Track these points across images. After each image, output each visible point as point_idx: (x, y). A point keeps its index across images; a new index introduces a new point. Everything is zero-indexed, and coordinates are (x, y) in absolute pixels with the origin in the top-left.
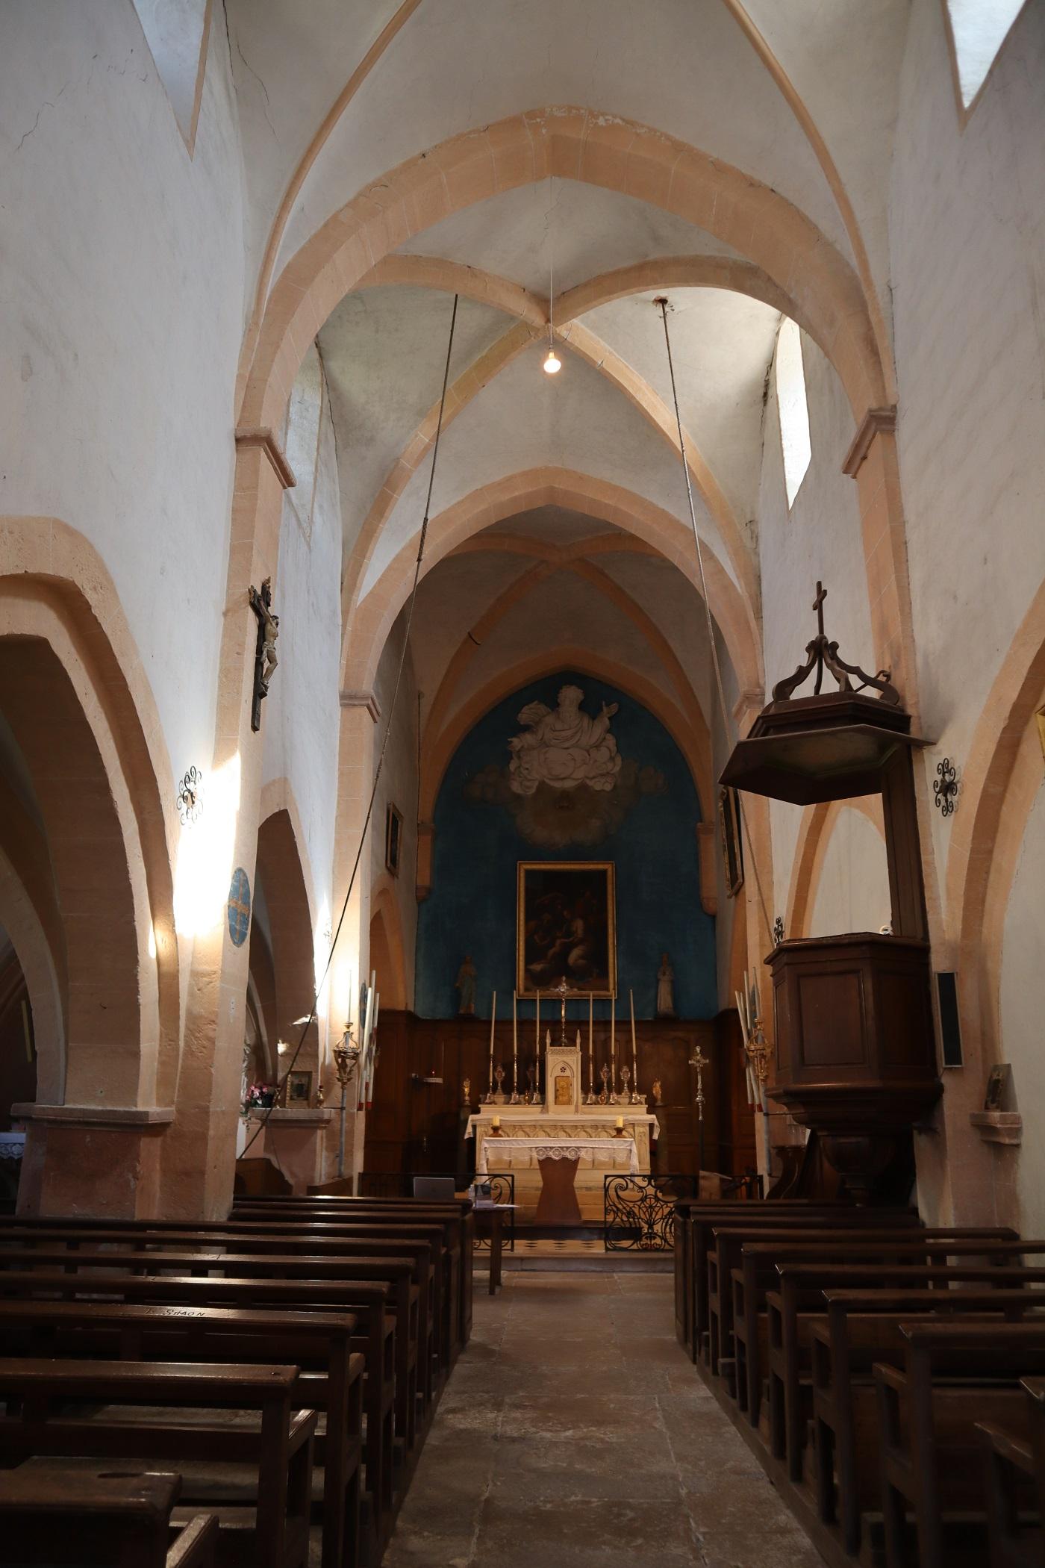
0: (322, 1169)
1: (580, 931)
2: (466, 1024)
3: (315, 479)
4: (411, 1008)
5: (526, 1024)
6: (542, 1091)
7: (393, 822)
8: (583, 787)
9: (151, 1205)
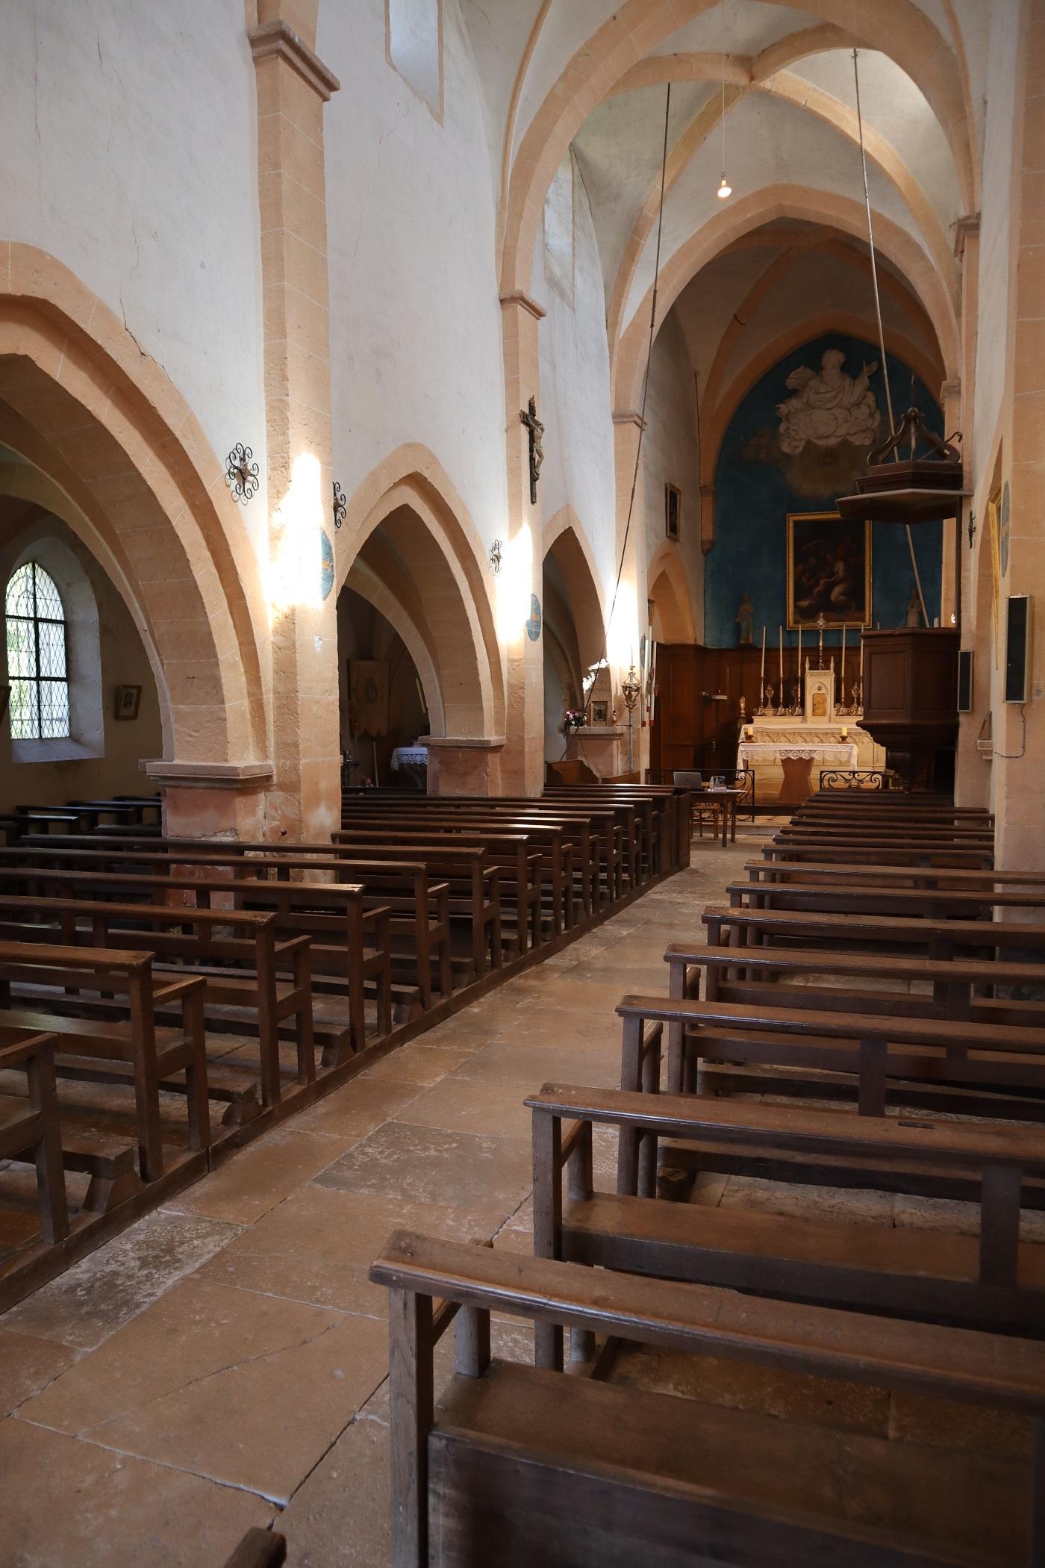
0: (619, 767)
1: (841, 573)
2: (746, 651)
3: (574, 248)
4: (701, 643)
5: (791, 651)
6: (803, 705)
7: (672, 497)
8: (845, 443)
9: (497, 788)
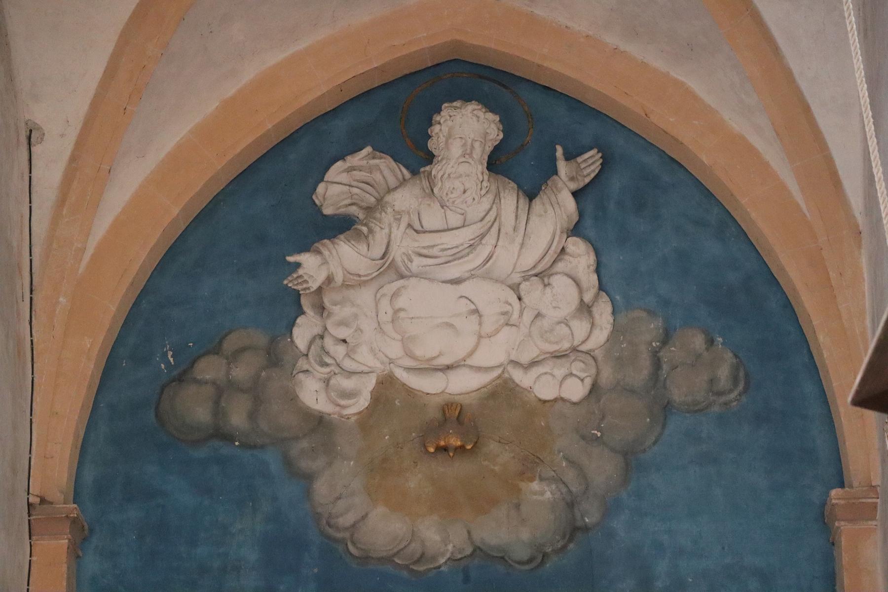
8: (503, 392)
